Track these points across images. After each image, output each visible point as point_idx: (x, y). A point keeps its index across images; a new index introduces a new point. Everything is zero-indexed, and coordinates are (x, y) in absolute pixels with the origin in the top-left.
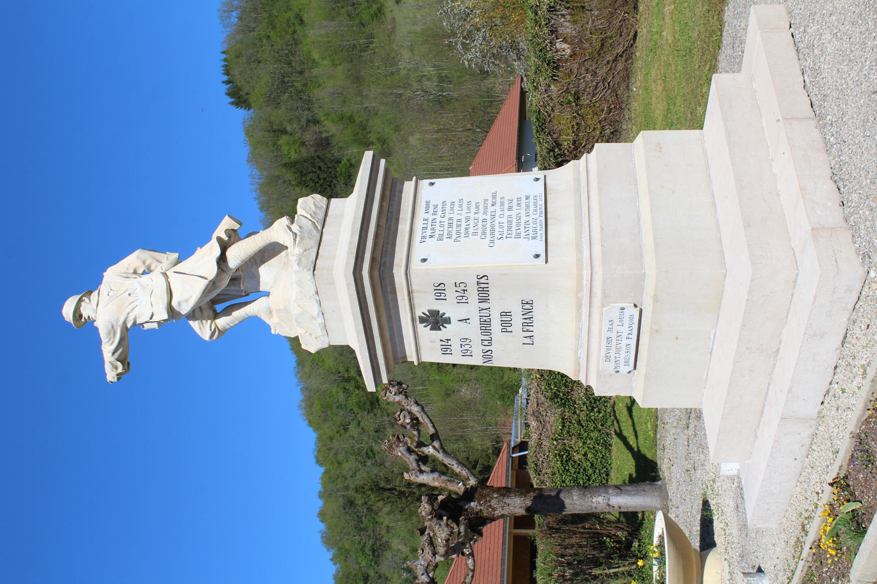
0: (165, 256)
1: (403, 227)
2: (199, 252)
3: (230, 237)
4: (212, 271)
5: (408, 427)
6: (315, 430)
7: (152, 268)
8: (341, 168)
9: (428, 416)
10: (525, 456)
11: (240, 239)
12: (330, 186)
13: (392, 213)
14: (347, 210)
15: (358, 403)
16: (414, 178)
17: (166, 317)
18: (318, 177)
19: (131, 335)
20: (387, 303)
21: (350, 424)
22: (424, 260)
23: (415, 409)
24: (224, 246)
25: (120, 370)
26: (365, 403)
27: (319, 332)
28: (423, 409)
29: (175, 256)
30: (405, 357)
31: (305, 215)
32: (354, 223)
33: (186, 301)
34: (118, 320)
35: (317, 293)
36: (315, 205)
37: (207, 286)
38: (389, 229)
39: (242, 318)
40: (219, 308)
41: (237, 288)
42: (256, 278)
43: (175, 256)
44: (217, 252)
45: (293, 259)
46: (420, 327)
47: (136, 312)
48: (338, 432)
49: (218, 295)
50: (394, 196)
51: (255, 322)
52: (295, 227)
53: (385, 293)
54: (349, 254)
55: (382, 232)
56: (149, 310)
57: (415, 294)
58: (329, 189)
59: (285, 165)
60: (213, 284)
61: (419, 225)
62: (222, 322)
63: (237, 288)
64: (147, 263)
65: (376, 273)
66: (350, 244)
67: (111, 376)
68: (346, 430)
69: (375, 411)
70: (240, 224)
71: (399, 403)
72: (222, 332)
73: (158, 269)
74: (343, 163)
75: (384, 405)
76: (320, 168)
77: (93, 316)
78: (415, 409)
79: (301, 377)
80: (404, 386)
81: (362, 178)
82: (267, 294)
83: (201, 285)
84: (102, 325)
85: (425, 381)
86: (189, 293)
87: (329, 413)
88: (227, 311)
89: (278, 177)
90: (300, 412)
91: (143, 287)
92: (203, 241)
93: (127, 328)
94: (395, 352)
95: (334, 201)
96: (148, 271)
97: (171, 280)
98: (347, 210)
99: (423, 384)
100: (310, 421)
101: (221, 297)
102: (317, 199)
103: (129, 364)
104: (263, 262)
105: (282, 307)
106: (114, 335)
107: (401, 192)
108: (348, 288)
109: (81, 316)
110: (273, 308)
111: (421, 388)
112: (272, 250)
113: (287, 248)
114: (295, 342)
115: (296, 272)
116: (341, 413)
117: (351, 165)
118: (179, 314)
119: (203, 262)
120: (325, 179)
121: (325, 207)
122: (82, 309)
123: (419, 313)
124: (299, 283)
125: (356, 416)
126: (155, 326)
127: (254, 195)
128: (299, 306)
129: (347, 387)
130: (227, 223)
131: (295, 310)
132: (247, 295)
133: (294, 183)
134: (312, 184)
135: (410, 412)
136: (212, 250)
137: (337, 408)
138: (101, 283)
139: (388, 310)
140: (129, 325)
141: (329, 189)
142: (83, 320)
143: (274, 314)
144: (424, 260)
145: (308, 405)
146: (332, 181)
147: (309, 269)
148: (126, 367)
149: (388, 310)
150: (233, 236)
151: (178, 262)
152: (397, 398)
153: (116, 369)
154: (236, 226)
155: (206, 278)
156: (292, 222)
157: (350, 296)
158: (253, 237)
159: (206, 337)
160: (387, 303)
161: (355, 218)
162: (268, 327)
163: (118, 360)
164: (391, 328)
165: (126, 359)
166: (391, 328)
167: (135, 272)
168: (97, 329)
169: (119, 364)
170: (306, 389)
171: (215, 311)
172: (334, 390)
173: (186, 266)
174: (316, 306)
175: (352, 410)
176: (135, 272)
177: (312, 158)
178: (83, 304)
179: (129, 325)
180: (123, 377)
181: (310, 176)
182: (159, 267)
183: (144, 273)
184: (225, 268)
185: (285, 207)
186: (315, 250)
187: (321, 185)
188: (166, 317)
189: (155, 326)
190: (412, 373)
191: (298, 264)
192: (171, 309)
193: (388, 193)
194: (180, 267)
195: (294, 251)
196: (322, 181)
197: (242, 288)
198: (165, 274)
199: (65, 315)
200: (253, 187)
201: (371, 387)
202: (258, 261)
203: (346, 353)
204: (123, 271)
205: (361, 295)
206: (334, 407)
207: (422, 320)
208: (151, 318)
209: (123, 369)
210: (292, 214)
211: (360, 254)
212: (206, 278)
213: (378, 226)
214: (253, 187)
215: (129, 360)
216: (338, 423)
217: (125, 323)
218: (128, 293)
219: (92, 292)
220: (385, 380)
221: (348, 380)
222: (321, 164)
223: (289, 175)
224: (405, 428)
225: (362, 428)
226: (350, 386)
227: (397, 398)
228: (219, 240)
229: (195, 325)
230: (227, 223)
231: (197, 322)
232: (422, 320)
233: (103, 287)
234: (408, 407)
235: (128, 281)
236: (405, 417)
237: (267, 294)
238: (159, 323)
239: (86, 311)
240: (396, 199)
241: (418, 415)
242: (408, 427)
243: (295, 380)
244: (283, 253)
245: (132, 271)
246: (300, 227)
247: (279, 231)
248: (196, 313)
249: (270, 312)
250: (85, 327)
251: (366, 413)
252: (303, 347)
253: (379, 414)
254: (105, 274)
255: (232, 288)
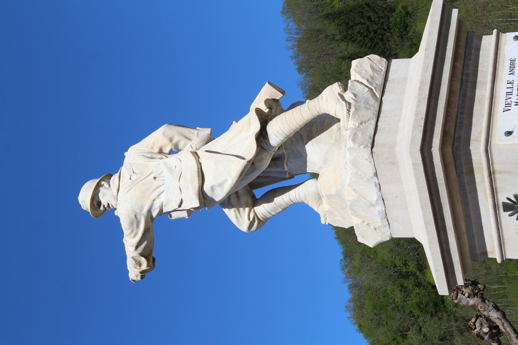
0: (196, 132)
1: (482, 93)
2: (235, 127)
3: (270, 108)
4: (249, 149)
5: (486, 337)
6: (366, 336)
7: (180, 147)
8: (395, 18)
9: (511, 325)
10: (326, 195)
11: (283, 111)
12: (382, 40)
13: (467, 75)
14: (412, 73)
15: (418, 305)
16: (495, 31)
17: (197, 204)
18: (368, 29)
19: (157, 226)
20: (462, 186)
21: (409, 329)
22: (509, 133)
23: (494, 315)
24: (264, 120)
25: (144, 267)
26: (427, 305)
27: (379, 221)
28: (504, 315)
29: (207, 131)
30: (485, 253)
31: (361, 80)
32: (420, 89)
33: (221, 185)
34: (142, 208)
35: (376, 174)
36: (372, 67)
37: (245, 167)
38: (464, 95)
39: (285, 206)
40: (258, 193)
41: (279, 170)
42: (302, 157)
43: (207, 131)
44: (256, 126)
45: (347, 134)
46: (504, 216)
47: (163, 198)
48: (395, 339)
49: (258, 177)
50: (470, 54)
51: (302, 211)
52: (348, 96)
53: (459, 175)
54: (415, 127)
55: (456, 99)
56: (178, 196)
57: (497, 176)
58: (380, 44)
59: (327, 16)
60: (252, 165)
61: (502, 89)
62: (263, 210)
63: (279, 170)
64: (175, 141)
65: (449, 150)
66: (416, 115)
67: (134, 274)
68: (404, 337)
69: (440, 314)
70: (283, 92)
71: (474, 307)
72: (262, 222)
73: (187, 148)
74: (397, 11)
75: (450, 308)
76: (369, 18)
77: (113, 203)
78: (494, 315)
79: (349, 272)
80: (479, 286)
81: (430, 34)
82: (315, 176)
83: (238, 166)
84: (123, 214)
85: (502, 278)
86: (223, 176)
87: (383, 316)
88: (268, 197)
89: (320, 31)
90: (348, 314)
91: (170, 169)
92: (240, 113)
93: (152, 217)
94: (472, 247)
95: (395, 62)
96: (175, 150)
97: (203, 160)
98: (412, 73)
99: (500, 282)
100: (360, 326)
101: (261, 180)
102: (375, 60)
103: (154, 260)
104: (310, 138)
105: (333, 192)
106: (138, 226)
107: (478, 49)
108: (415, 169)
109: (99, 203)
110: (323, 193)
111: (496, 286)
112: (321, 124)
113: (338, 120)
114: (347, 235)
115: (351, 149)
116: (398, 316)
117: (408, 13)
118: (212, 200)
119: (240, 139)
120: (375, 32)
121: (384, 70)
122: (100, 195)
123: (502, 199)
124: (355, 163)
125: (416, 320)
126: (185, 215)
127: (291, 53)
128: (354, 190)
129: (405, 284)
130: (267, 92)
131: (349, 196)
132: (292, 177)
133: (338, 37)
134: (360, 38)
135: (488, 320)
136: (250, 124)
137: (393, 309)
138: (121, 164)
139: (464, 195)
140: (154, 214)
141: (380, 44)
142: (102, 208)
143: (324, 200)
144: (509, 133)
145: (358, 306)
146: (393, 39)
147: (366, 146)
148: (151, 263)
149: (464, 195)
150: (275, 108)
151: (210, 139)
152: (472, 302)
153: (140, 265)
154: (278, 96)
155: (243, 158)
156: (345, 89)
157: (417, 179)
158: (298, 108)
159: (244, 226)
160: (462, 186)
161: (422, 82)
162: (317, 216)
163: (142, 255)
164: (468, 217)
165: (151, 253)
166: (468, 217)
167: (161, 152)
168: (118, 219)
169: (144, 261)
170: (356, 286)
171: (253, 196)
172: (389, 288)
173: (220, 143)
174: (375, 190)
175: (411, 312)
176: (161, 152)
177: (360, 6)
178: (101, 189)
179: (154, 214)
180: (147, 275)
181: (357, 28)
182: (188, 146)
183: (171, 152)
184: (265, 146)
185: (328, 67)
186: (374, 122)
187: (371, 39)
188: (197, 204)
189: (185, 215)
190: (486, 268)
191: (354, 140)
192: (202, 195)
193: (462, 51)
194: (212, 145)
195: (347, 124)
196: (372, 34)
197: (286, 169)
198: (195, 154)
199: (81, 203)
200: (290, 44)
201: (443, 290)
202: (305, 137)
203: (409, 249)
204: (147, 150)
205: (431, 177)
206: (389, 308)
207: (507, 207)
208: (180, 206)
209: (148, 265)
210: (343, 77)
211: (429, 127)
212: (243, 158)
213: (450, 92)
214: (290, 44)
215: (154, 255)
216: (395, 328)
217: (150, 211)
218: (152, 176)
219: (111, 176)
220: (460, 281)
221: (406, 276)
222: (371, 14)
223: (332, 29)
224: (482, 338)
225: (425, 335)
226: (409, 283)
227: (472, 302)
228: (259, 112)
229: (230, 213)
230: (267, 92)
231: (232, 210)
232: (507, 207)
233: (124, 170)
234: (486, 313)
235: (152, 163)
236: (481, 325)
237: (315, 176)
238: (189, 211)
239: (106, 197)
240: (473, 57)
241: (498, 323)
242: (486, 337)
243: (341, 276)
244: (335, 127)
245: (157, 150)
246: (355, 95)
247: (329, 100)
248: (232, 200)
249: (319, 198)
250: (104, 217)
251: (429, 316)
252: (360, 240)
253: (445, 318)
254: (126, 154)
255: (274, 169)
